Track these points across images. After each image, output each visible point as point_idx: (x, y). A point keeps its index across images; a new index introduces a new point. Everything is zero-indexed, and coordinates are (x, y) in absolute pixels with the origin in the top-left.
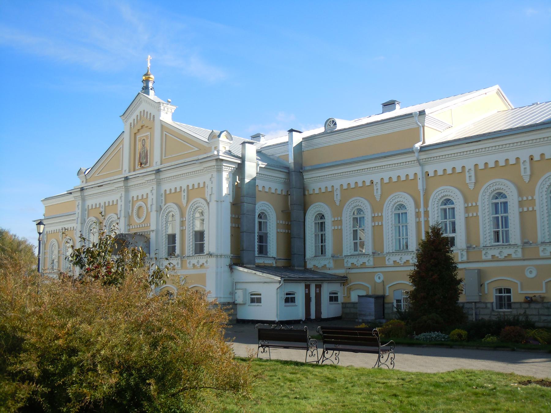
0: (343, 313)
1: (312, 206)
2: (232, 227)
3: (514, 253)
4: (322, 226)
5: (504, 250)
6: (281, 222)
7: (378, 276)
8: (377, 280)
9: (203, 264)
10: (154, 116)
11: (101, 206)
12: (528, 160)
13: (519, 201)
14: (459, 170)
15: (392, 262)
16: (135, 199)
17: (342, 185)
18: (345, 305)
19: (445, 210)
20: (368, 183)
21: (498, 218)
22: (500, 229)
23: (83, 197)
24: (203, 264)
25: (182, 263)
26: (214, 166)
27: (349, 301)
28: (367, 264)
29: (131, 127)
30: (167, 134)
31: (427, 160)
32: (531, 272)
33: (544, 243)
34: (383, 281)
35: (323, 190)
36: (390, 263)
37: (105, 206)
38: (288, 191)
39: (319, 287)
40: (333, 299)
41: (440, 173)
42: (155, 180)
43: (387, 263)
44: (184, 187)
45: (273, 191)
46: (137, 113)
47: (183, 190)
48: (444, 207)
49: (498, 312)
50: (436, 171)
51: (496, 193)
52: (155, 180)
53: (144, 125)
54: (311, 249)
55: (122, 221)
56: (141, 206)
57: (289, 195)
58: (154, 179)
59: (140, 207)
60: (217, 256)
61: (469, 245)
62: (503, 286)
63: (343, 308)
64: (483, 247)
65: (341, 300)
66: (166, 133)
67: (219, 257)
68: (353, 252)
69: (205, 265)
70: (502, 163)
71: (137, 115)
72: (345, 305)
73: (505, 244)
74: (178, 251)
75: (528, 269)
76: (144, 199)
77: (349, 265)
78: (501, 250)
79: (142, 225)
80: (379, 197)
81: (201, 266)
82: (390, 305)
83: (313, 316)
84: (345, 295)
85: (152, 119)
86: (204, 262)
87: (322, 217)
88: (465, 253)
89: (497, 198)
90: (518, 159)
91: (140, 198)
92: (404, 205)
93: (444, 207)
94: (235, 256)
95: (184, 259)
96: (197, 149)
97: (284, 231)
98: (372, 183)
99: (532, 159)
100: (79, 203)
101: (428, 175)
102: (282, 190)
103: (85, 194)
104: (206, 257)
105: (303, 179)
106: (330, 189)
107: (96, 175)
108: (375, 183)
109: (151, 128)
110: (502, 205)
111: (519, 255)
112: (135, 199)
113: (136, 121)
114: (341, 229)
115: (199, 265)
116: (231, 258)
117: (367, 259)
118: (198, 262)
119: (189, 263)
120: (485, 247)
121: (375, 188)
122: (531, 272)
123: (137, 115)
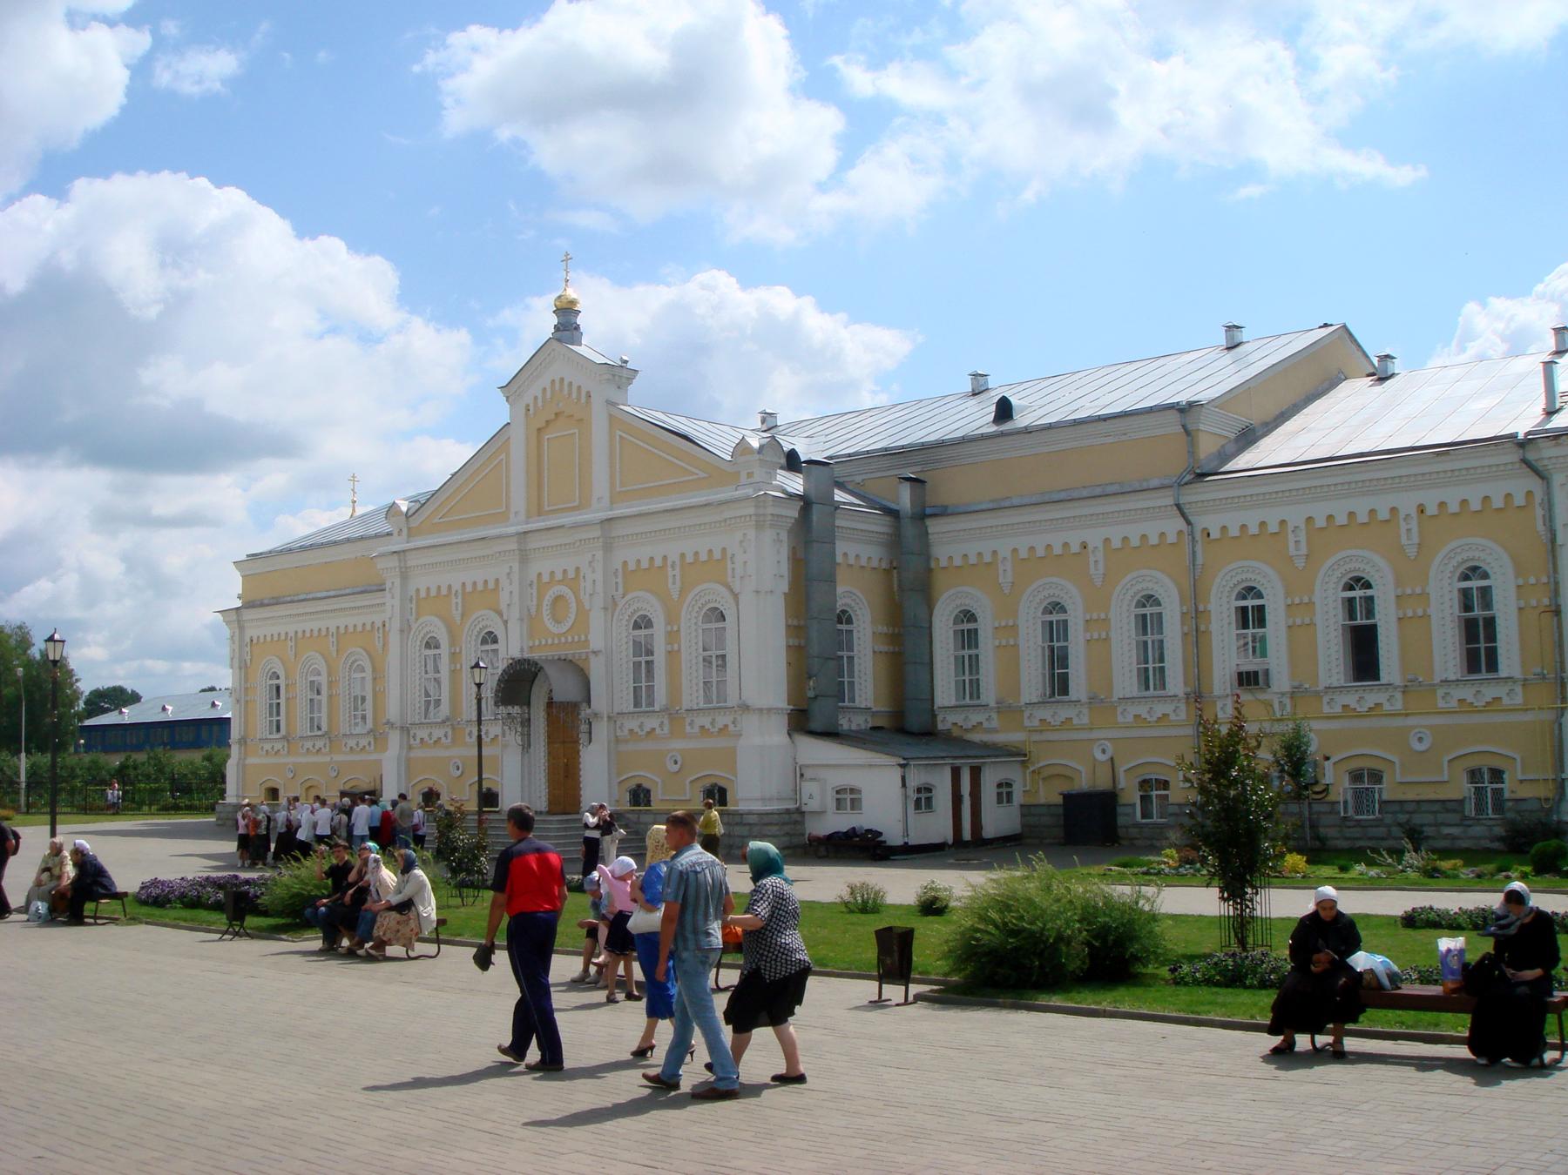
0: (1023, 826)
1: (946, 595)
2: (789, 647)
3: (1388, 700)
4: (968, 638)
5: (1484, 689)
6: (885, 629)
7: (1101, 748)
8: (1100, 757)
9: (320, 748)
10: (589, 395)
11: (454, 592)
12: (1414, 512)
13: (1397, 596)
14: (1273, 527)
15: (1130, 718)
16: (546, 578)
17: (1015, 550)
18: (1026, 809)
19: (1144, 616)
20: (1075, 548)
21: (1145, 643)
22: (1150, 666)
23: (403, 570)
24: (320, 748)
25: (289, 748)
26: (750, 516)
27: (1035, 802)
28: (1506, 701)
29: (527, 415)
30: (624, 435)
31: (1206, 504)
32: (1420, 739)
33: (1446, 681)
34: (1112, 759)
35: (973, 560)
36: (1127, 721)
37: (464, 593)
38: (891, 563)
39: (976, 772)
40: (1005, 792)
41: (1234, 531)
42: (601, 540)
43: (1120, 719)
44: (457, 587)
45: (863, 562)
46: (545, 381)
47: (669, 563)
48: (1049, 618)
49: (1357, 820)
50: (1224, 528)
51: (1351, 579)
52: (601, 540)
53: (564, 412)
54: (945, 692)
55: (515, 628)
56: (563, 596)
57: (895, 568)
58: (598, 538)
59: (558, 599)
60: (761, 710)
61: (1296, 684)
62: (1486, 763)
63: (1023, 815)
64: (1326, 688)
65: (1018, 798)
66: (620, 433)
67: (765, 712)
68: (632, 708)
69: (730, 729)
70: (1135, 542)
71: (545, 389)
72: (1026, 809)
73: (644, 708)
74: (661, 698)
75: (1416, 733)
76: (573, 580)
77: (1036, 723)
78: (1512, 688)
79: (566, 638)
80: (1101, 579)
81: (648, 733)
82: (1129, 810)
83: (967, 835)
84: (1028, 788)
85: (574, 395)
86: (322, 746)
87: (969, 616)
88: (1287, 701)
89: (1144, 606)
90: (1393, 510)
91: (559, 576)
92: (1157, 596)
93: (1049, 618)
94: (796, 708)
95: (460, 726)
96: (702, 475)
97: (891, 648)
98: (1085, 548)
99: (1422, 511)
100: (393, 583)
101: (1209, 535)
102: (881, 559)
103: (409, 563)
104: (722, 714)
105: (927, 533)
106: (988, 558)
107: (436, 520)
108: (1090, 547)
109: (581, 420)
110: (1363, 600)
111: (1398, 705)
112: (546, 578)
113: (540, 401)
114: (1016, 646)
115: (432, 741)
116: (789, 714)
117: (1386, 695)
118: (641, 726)
119: (691, 724)
120: (1329, 688)
121: (1092, 559)
122: (1420, 739)
123: (545, 389)
